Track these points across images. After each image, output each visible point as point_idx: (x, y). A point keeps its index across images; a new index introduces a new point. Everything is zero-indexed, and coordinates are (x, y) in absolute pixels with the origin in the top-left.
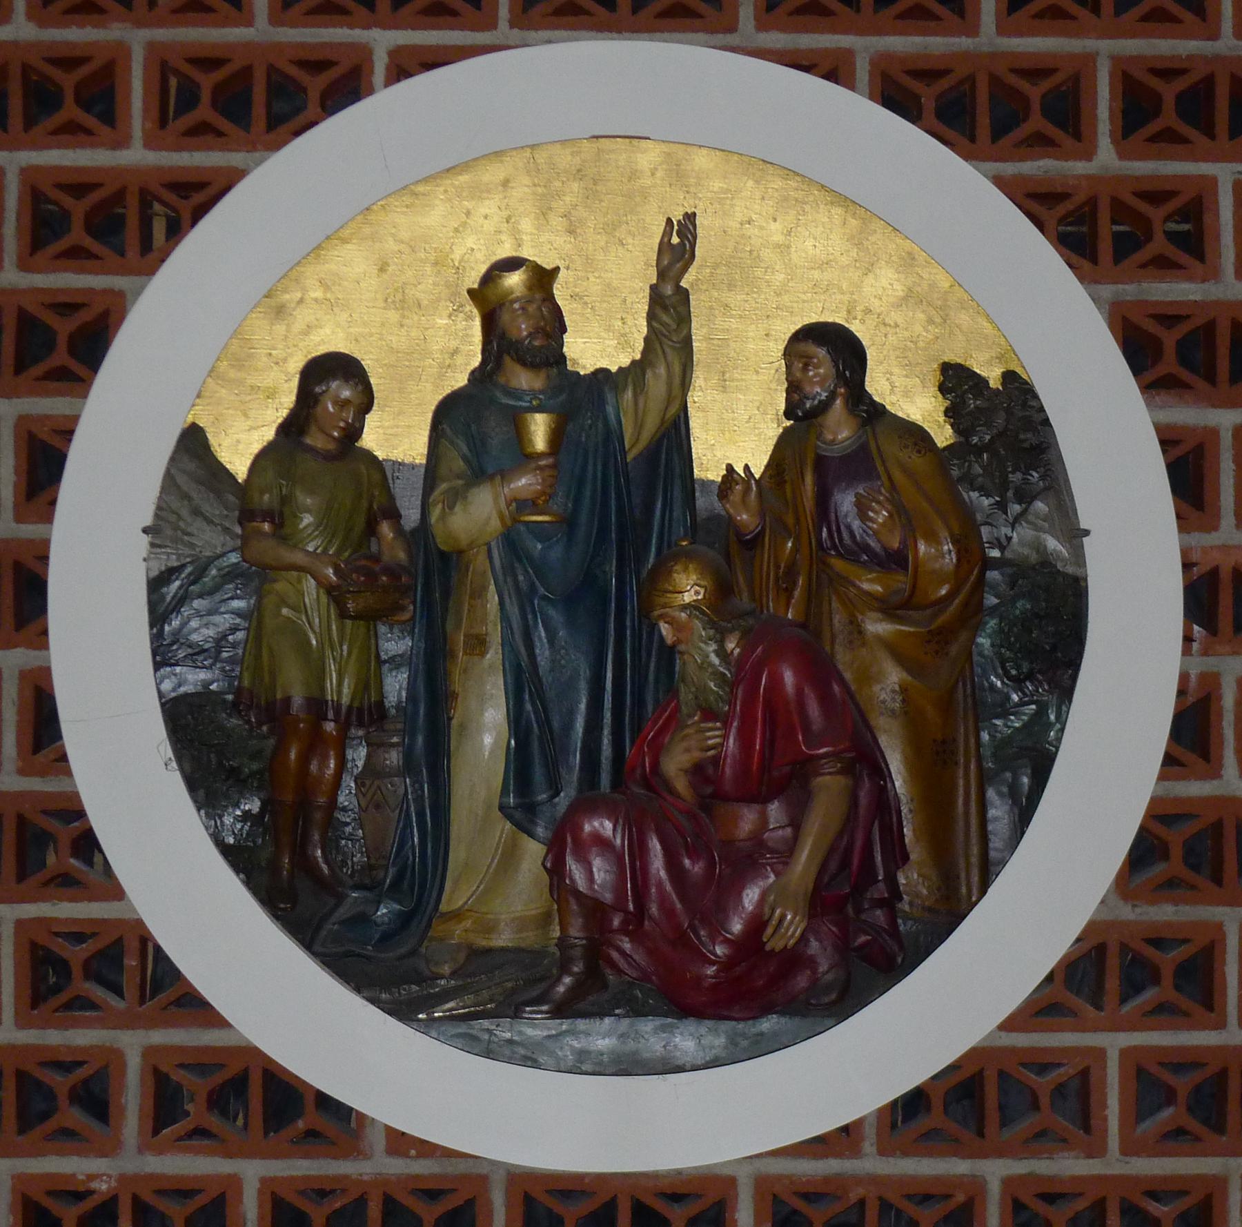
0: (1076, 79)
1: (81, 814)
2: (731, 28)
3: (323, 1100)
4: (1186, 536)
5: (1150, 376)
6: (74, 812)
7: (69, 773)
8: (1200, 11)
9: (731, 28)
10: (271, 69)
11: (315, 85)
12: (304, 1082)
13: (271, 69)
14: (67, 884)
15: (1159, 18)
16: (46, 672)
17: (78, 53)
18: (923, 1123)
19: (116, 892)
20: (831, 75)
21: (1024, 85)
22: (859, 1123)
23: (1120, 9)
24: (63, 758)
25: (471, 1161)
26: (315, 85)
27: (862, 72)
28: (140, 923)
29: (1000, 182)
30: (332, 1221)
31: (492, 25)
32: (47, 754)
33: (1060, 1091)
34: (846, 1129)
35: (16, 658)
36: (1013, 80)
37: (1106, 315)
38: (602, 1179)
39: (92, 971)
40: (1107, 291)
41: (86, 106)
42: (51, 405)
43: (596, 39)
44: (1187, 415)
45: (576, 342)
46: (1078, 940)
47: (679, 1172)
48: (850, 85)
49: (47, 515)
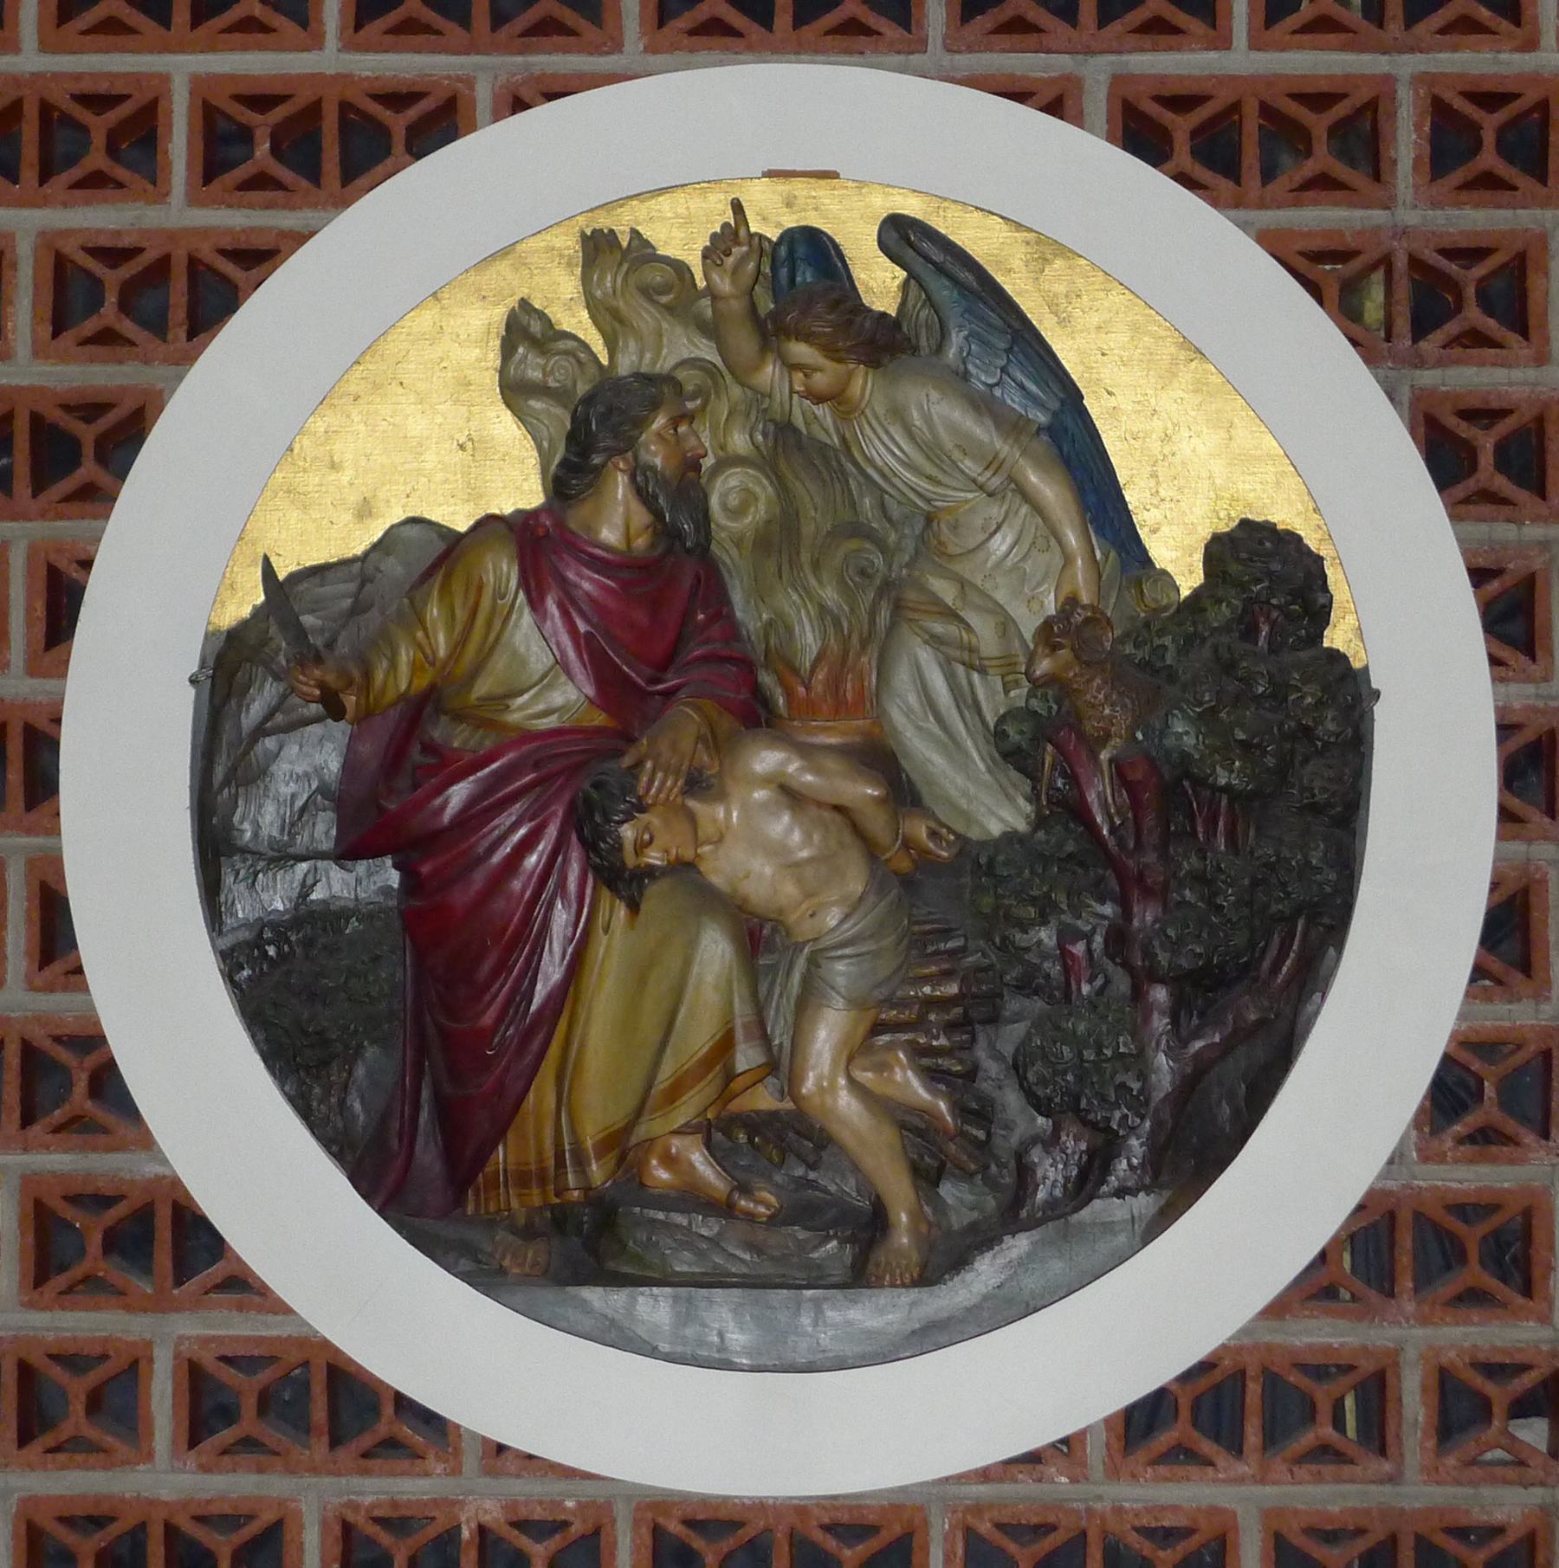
0: (1372, 106)
1: (102, 1039)
2: (921, 45)
3: (403, 1403)
4: (1502, 688)
5: (1460, 491)
6: (91, 1041)
7: (85, 989)
8: (596, 17)
9: (921, 45)
10: (345, 107)
11: (398, 123)
12: (382, 1382)
13: (345, 107)
14: (76, 1127)
15: (1158, 29)
16: (55, 862)
17: (1195, 89)
18: (1165, 1439)
19: (146, 1141)
20: (1055, 108)
21: (1167, 117)
22: (1081, 1435)
23: (499, 19)
24: (79, 970)
25: (601, 1483)
26: (398, 123)
27: (1097, 102)
28: (176, 1183)
29: (1275, 244)
30: (241, 1556)
31: (617, 46)
32: (57, 967)
33: (228, 1415)
34: (1065, 1441)
35: (16, 845)
36: (1153, 109)
37: (1406, 414)
38: (760, 1506)
39: (112, 1242)
40: (151, 1169)
41: (1345, 155)
42: (67, 529)
43: (688, 67)
44: (57, 1003)
45: (958, 446)
46: (1361, 1208)
47: (726, 1499)
48: (1078, 120)
49: (60, 669)
